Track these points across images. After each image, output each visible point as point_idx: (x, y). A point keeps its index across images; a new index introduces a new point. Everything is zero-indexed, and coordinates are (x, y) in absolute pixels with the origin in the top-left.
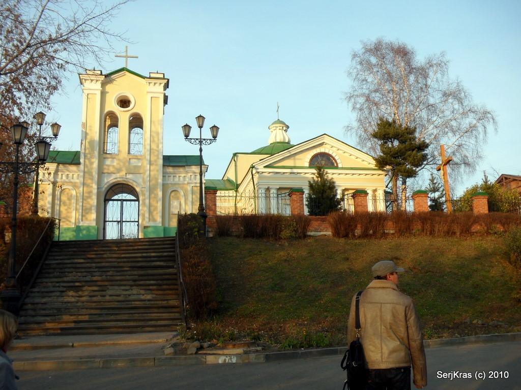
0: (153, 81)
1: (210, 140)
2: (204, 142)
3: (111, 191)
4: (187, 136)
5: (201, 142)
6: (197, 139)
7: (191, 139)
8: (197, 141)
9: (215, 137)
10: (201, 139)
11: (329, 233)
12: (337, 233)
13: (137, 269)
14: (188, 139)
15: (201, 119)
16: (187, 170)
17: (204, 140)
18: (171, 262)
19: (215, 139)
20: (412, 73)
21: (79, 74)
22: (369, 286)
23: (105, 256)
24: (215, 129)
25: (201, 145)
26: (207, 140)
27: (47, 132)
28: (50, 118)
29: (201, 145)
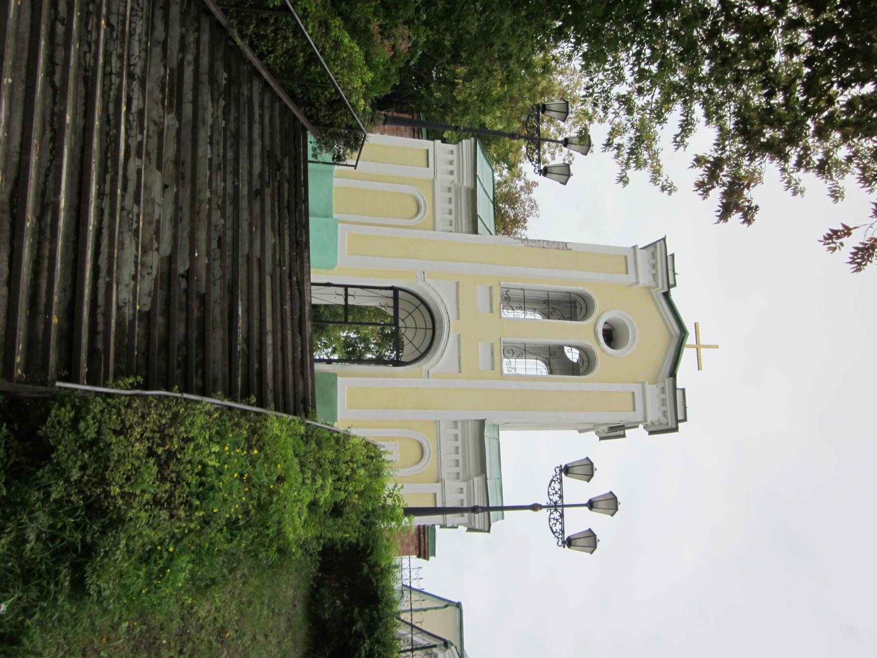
0: (668, 396)
1: (563, 532)
2: (556, 515)
3: (418, 302)
4: (566, 470)
5: (555, 506)
6: (561, 497)
7: (561, 482)
8: (556, 498)
9: (569, 542)
10: (563, 506)
13: (228, 276)
14: (560, 474)
15: (609, 504)
16: (666, 381)
17: (562, 516)
18: (245, 331)
19: (563, 542)
21: (664, 239)
23: (269, 232)
24: (590, 541)
25: (548, 507)
26: (562, 524)
27: (554, 157)
28: (579, 162)
29: (548, 507)
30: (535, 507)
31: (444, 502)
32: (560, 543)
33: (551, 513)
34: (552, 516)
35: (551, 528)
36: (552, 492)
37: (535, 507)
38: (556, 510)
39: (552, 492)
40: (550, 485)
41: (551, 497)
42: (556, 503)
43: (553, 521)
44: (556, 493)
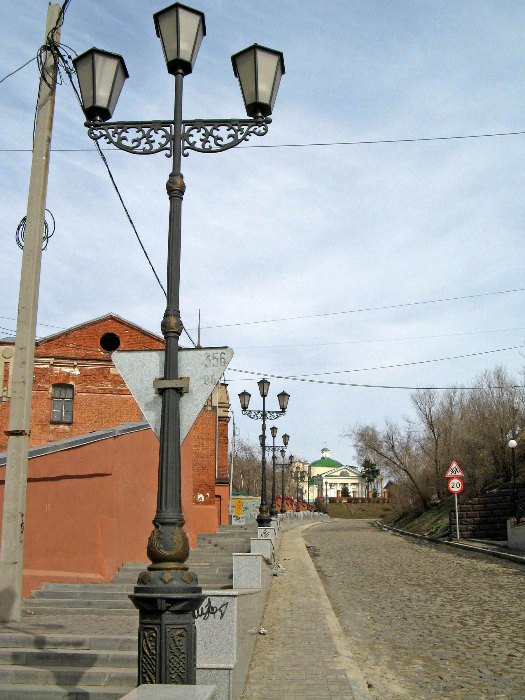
1: (277, 412)
4: (244, 408)
5: (264, 417)
6: (259, 412)
8: (259, 415)
9: (283, 409)
10: (264, 411)
11: (346, 501)
12: (348, 502)
15: (263, 384)
20: (378, 471)
22: (268, 117)
25: (264, 420)
26: (273, 412)
29: (264, 420)
30: (175, 190)
31: (123, 645)
32: (261, 129)
33: (192, 146)
34: (199, 145)
35: (275, 418)
36: (256, 417)
37: (175, 190)
38: (186, 136)
39: (256, 417)
40: (253, 418)
41: (156, 146)
42: (262, 415)
43: (211, 143)
44: (257, 414)
